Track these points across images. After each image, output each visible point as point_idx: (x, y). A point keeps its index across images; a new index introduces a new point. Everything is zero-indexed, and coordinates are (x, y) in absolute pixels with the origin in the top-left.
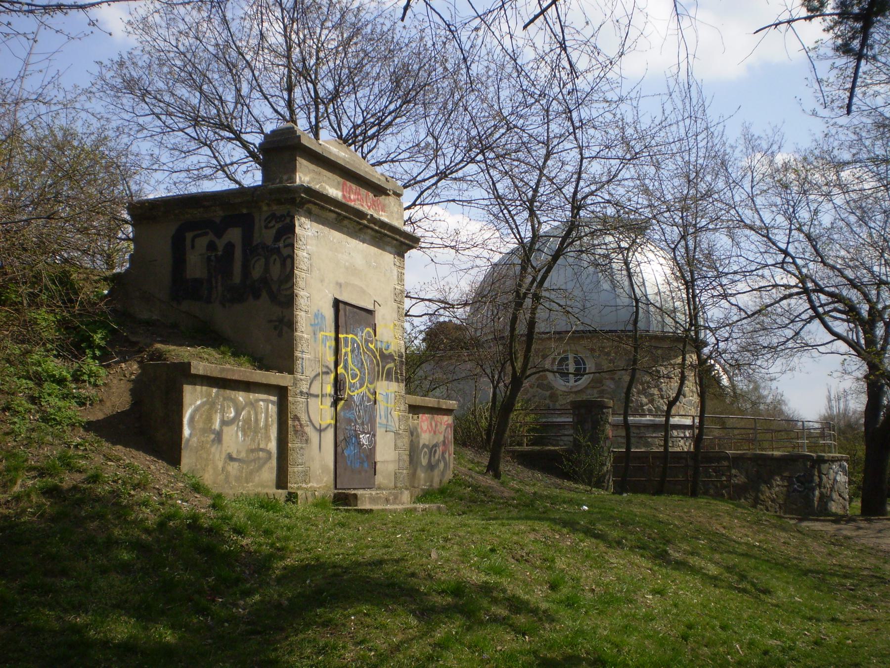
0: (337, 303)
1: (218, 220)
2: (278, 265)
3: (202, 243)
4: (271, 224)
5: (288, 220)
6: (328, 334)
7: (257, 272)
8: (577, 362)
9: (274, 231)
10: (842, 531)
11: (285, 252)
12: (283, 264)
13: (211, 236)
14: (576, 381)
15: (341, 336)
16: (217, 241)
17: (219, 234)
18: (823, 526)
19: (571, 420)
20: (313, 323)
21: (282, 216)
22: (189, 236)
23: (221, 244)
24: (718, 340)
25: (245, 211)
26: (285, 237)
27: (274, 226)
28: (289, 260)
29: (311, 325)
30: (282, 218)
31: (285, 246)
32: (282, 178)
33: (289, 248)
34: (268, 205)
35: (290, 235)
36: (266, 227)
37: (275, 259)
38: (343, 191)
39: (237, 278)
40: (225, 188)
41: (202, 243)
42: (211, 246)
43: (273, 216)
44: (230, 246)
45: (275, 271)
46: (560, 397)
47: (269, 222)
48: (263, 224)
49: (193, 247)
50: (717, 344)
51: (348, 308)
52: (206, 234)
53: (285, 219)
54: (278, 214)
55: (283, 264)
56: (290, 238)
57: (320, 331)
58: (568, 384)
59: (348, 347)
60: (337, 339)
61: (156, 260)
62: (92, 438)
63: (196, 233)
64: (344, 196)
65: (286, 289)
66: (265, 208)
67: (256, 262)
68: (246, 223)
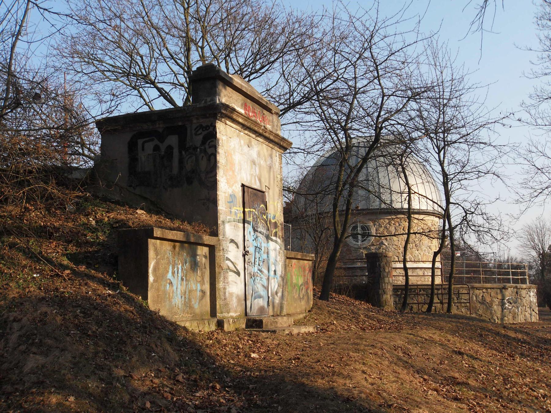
0: (243, 186)
1: (161, 130)
2: (205, 159)
3: (150, 147)
4: (199, 132)
5: (211, 129)
6: (238, 209)
7: (189, 166)
8: (363, 228)
9: (201, 137)
10: (276, 305)
11: (210, 151)
12: (209, 160)
13: (156, 142)
14: (362, 241)
15: (246, 210)
16: (160, 145)
17: (162, 139)
18: (248, 299)
19: (366, 266)
20: (229, 201)
21: (207, 126)
22: (140, 142)
23: (163, 147)
24: (466, 214)
25: (180, 124)
26: (209, 141)
27: (201, 133)
28: (212, 157)
29: (228, 202)
30: (207, 128)
31: (210, 147)
32: (206, 100)
33: (213, 149)
34: (197, 119)
35: (212, 140)
36: (196, 135)
37: (203, 156)
38: (245, 110)
39: (175, 171)
40: (164, 108)
41: (150, 147)
42: (156, 148)
43: (201, 127)
44: (170, 148)
45: (203, 164)
46: (353, 251)
47: (198, 131)
48: (193, 132)
49: (143, 149)
50: (466, 216)
51: (250, 190)
52: (152, 140)
53: (209, 128)
54: (204, 125)
55: (209, 160)
56: (212, 141)
57: (234, 206)
58: (357, 243)
59: (250, 218)
60: (244, 212)
61: (117, 159)
62: (440, 350)
63: (145, 140)
64: (245, 113)
65: (211, 177)
66: (195, 121)
67: (189, 158)
68: (181, 132)
